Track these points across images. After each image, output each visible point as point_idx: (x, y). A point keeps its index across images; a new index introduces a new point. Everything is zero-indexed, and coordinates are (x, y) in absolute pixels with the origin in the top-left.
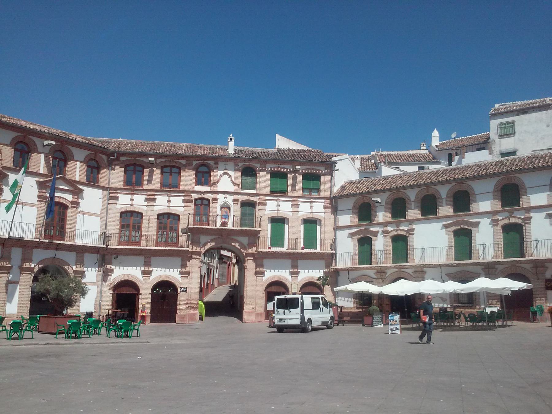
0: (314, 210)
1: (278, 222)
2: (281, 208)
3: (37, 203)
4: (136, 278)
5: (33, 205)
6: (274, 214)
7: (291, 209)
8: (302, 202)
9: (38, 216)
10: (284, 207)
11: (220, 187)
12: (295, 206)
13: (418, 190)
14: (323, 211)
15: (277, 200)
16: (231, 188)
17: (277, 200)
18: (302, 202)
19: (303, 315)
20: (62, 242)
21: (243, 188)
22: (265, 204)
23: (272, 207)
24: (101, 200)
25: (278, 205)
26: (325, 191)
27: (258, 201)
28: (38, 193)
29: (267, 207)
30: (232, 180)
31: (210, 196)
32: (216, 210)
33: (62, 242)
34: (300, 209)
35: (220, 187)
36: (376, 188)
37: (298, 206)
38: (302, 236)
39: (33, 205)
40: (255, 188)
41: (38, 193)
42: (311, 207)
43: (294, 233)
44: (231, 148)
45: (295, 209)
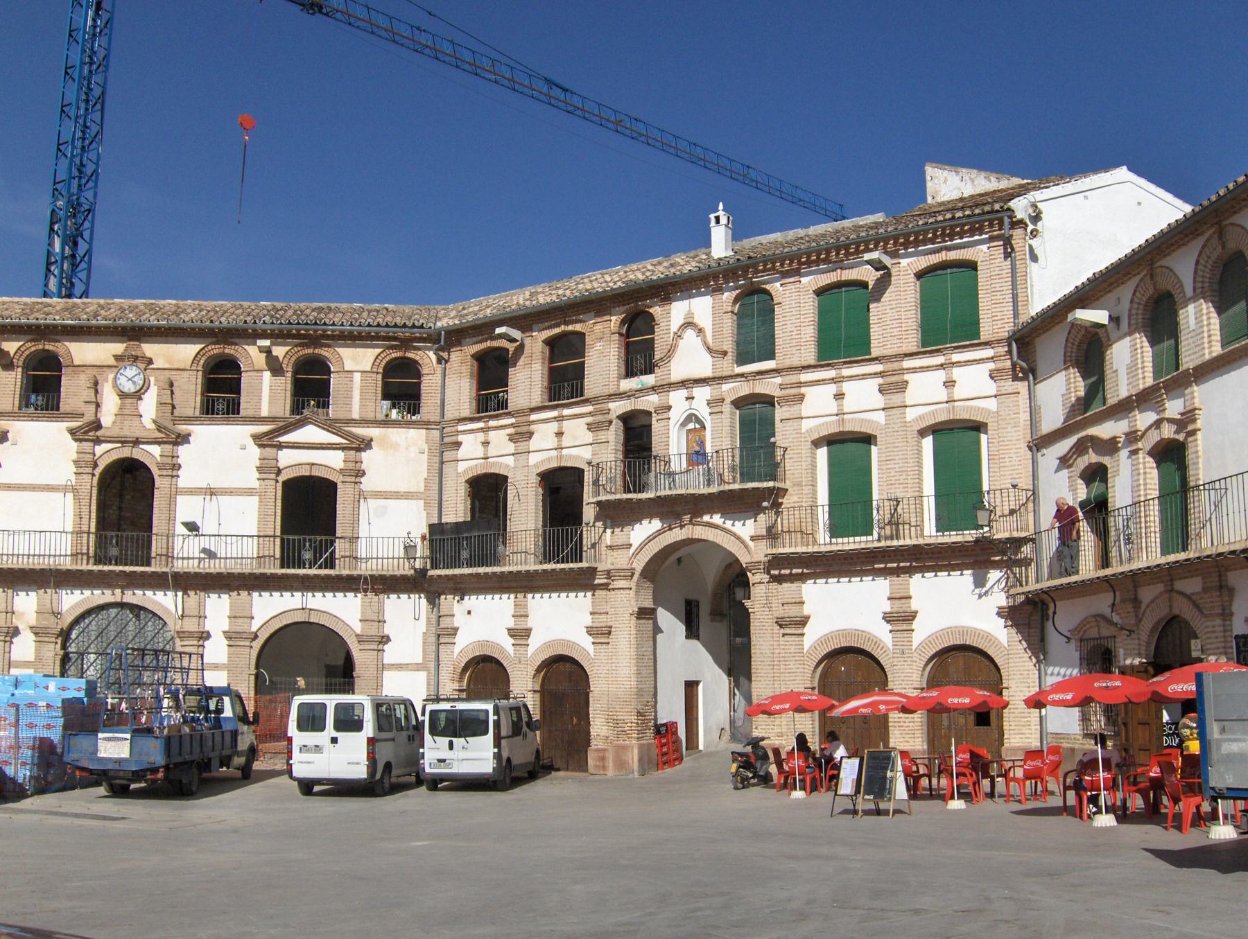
0: (958, 392)
1: (849, 446)
2: (849, 404)
3: (256, 484)
4: (989, 637)
5: (249, 492)
6: (831, 427)
7: (879, 401)
8: (914, 370)
9: (262, 517)
10: (858, 398)
11: (679, 368)
12: (893, 386)
13: (1195, 246)
14: (991, 387)
15: (833, 381)
16: (704, 366)
17: (833, 381)
18: (914, 370)
19: (373, 749)
20: (497, 569)
21: (742, 359)
22: (801, 398)
23: (824, 403)
24: (425, 456)
25: (839, 396)
26: (996, 319)
27: (776, 393)
28: (75, 470)
29: (806, 408)
30: (705, 343)
31: (649, 402)
32: (671, 442)
33: (497, 569)
34: (911, 396)
35: (679, 368)
36: (175, 321)
37: (902, 387)
38: (929, 487)
39: (249, 492)
40: (771, 355)
41: (75, 470)
42: (949, 384)
43: (905, 479)
44: (720, 245)
45: (896, 399)
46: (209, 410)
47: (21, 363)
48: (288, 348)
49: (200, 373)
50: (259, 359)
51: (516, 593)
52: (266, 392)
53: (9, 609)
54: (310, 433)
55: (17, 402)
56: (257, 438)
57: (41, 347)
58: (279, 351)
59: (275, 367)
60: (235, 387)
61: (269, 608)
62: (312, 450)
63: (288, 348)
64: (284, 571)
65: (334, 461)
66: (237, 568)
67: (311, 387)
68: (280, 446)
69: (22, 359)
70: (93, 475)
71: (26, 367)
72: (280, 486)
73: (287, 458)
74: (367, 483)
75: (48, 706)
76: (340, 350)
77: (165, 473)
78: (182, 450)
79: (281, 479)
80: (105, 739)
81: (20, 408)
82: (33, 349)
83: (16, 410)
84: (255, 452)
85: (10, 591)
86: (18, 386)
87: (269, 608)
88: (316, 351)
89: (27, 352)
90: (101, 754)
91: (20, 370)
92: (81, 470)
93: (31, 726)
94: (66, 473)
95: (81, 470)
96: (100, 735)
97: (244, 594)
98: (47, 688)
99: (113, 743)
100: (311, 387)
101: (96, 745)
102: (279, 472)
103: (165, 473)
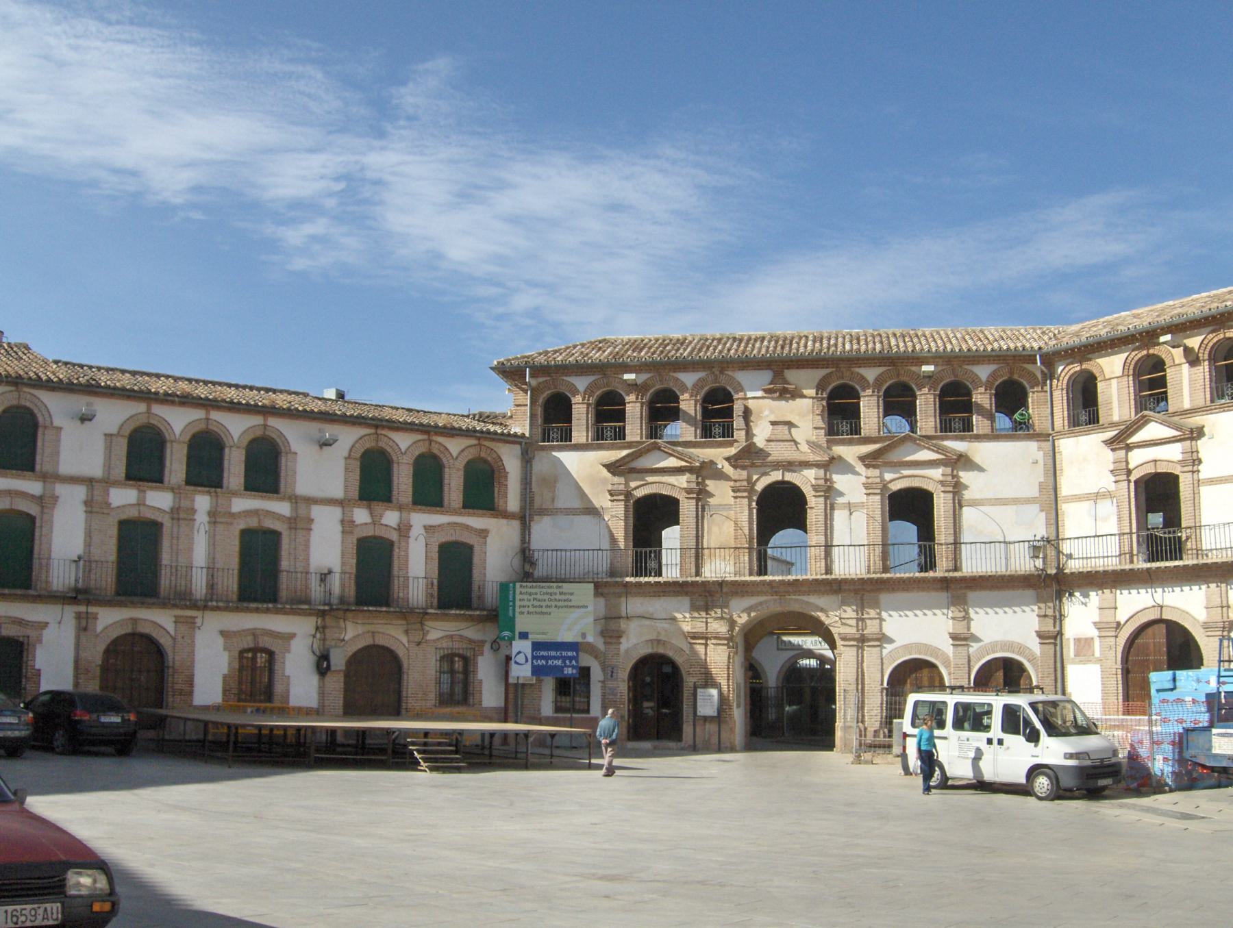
3: (1112, 487)
28: (1114, 479)
46: (1074, 422)
47: (1206, 356)
48: (1126, 354)
49: (1131, 378)
50: (1178, 353)
51: (1207, 583)
52: (1116, 396)
53: (1225, 604)
54: (1153, 430)
55: (1208, 396)
56: (1109, 443)
57: (1222, 336)
58: (1194, 342)
59: (1192, 359)
60: (1162, 382)
61: (1134, 604)
62: (1156, 450)
63: (1126, 354)
64: (1149, 565)
65: (1173, 453)
66: (1099, 565)
67: (1151, 386)
68: (1129, 448)
69: (1207, 352)
70: (1129, 481)
71: (1213, 359)
72: (1132, 485)
73: (1137, 458)
74: (1205, 471)
75: (1194, 701)
76: (1098, 360)
77: (1186, 469)
78: (1202, 444)
79: (1133, 478)
80: (1218, 735)
81: (1212, 401)
82: (1215, 340)
83: (1208, 403)
84: (1108, 456)
85: (1223, 585)
86: (1207, 380)
87: (1134, 604)
88: (1151, 351)
89: (1211, 344)
90: (1215, 751)
91: (1206, 363)
92: (1118, 478)
93: (1165, 721)
94: (1107, 482)
95: (1118, 478)
96: (1214, 731)
97: (1107, 591)
98: (1208, 682)
99: (1226, 739)
100: (1151, 386)
101: (1210, 741)
102: (1129, 472)
103: (1186, 469)
